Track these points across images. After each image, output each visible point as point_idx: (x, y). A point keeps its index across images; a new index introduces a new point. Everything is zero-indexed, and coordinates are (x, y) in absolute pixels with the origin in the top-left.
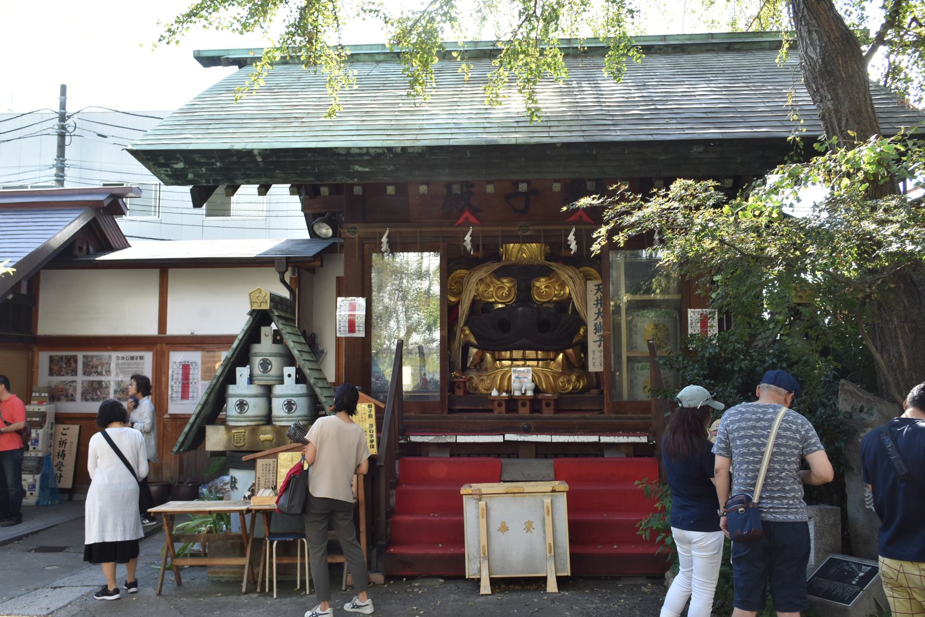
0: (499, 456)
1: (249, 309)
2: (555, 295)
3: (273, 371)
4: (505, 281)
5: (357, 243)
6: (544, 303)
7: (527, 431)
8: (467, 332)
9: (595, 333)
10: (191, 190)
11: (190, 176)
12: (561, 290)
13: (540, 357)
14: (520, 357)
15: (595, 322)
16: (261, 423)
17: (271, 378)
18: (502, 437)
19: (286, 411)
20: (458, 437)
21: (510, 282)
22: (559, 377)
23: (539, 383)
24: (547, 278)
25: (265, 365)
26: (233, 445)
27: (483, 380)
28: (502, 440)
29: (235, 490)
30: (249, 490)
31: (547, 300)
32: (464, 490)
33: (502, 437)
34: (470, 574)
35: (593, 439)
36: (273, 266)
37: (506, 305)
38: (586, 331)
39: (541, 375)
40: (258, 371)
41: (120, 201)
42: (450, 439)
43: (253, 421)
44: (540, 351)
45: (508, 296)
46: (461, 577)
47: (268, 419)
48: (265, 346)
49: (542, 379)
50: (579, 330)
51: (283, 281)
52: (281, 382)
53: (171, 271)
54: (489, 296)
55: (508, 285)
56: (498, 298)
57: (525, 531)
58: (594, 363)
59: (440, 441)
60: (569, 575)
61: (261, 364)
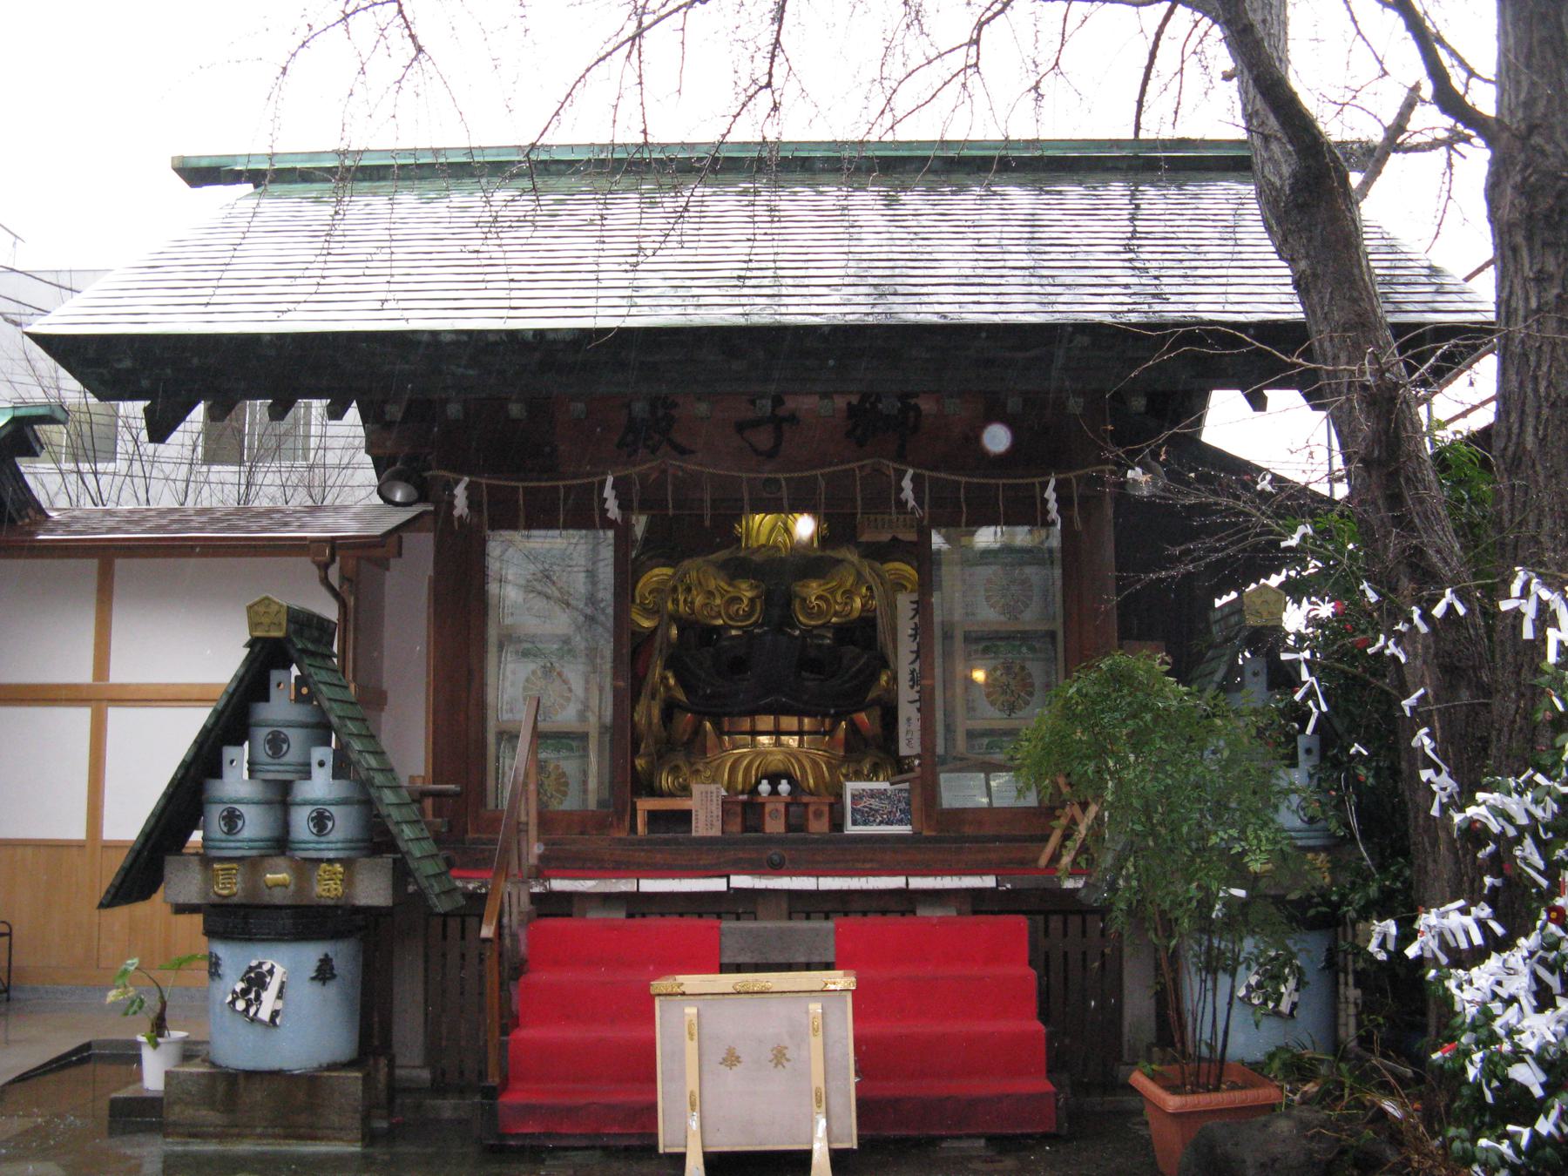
0: (719, 916)
1: (248, 638)
2: (836, 614)
3: (293, 755)
4: (744, 586)
5: (522, 515)
6: (815, 627)
7: (777, 869)
8: (672, 681)
9: (912, 687)
10: (146, 410)
11: (145, 383)
12: (846, 604)
13: (806, 728)
14: (795, 728)
15: (912, 667)
16: (270, 852)
17: (288, 768)
18: (725, 880)
19: (315, 831)
20: (641, 881)
21: (752, 587)
22: (839, 767)
23: (802, 776)
24: (822, 582)
25: (277, 743)
26: (216, 893)
27: (698, 771)
28: (724, 888)
29: (217, 979)
30: (242, 980)
31: (820, 622)
32: (660, 985)
33: (724, 881)
34: (668, 1143)
35: (897, 882)
36: (308, 555)
37: (745, 632)
38: (894, 679)
39: (808, 766)
40: (263, 754)
41: (28, 430)
42: (625, 886)
43: (251, 848)
44: (808, 715)
45: (748, 615)
46: (648, 1147)
47: (281, 843)
48: (280, 707)
49: (809, 771)
50: (878, 680)
51: (325, 581)
52: (307, 775)
53: (119, 563)
54: (713, 614)
55: (749, 594)
56: (731, 618)
57: (773, 1064)
58: (909, 741)
59: (607, 890)
60: (855, 1147)
61: (269, 742)
